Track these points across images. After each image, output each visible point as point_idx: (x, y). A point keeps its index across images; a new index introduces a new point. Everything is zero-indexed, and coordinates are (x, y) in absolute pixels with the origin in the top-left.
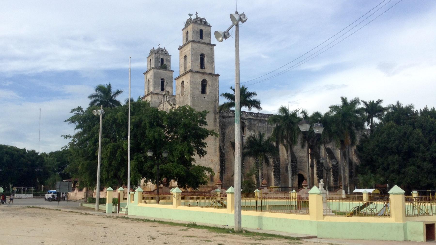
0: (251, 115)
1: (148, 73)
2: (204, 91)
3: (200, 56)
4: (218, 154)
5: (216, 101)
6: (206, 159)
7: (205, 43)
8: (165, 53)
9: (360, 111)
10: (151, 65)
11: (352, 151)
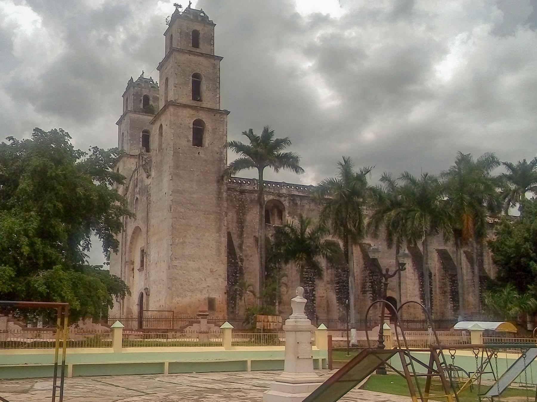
1: (123, 121)
2: (198, 141)
3: (191, 78)
4: (224, 257)
5: (222, 159)
6: (199, 268)
7: (202, 55)
9: (499, 181)
10: (127, 107)
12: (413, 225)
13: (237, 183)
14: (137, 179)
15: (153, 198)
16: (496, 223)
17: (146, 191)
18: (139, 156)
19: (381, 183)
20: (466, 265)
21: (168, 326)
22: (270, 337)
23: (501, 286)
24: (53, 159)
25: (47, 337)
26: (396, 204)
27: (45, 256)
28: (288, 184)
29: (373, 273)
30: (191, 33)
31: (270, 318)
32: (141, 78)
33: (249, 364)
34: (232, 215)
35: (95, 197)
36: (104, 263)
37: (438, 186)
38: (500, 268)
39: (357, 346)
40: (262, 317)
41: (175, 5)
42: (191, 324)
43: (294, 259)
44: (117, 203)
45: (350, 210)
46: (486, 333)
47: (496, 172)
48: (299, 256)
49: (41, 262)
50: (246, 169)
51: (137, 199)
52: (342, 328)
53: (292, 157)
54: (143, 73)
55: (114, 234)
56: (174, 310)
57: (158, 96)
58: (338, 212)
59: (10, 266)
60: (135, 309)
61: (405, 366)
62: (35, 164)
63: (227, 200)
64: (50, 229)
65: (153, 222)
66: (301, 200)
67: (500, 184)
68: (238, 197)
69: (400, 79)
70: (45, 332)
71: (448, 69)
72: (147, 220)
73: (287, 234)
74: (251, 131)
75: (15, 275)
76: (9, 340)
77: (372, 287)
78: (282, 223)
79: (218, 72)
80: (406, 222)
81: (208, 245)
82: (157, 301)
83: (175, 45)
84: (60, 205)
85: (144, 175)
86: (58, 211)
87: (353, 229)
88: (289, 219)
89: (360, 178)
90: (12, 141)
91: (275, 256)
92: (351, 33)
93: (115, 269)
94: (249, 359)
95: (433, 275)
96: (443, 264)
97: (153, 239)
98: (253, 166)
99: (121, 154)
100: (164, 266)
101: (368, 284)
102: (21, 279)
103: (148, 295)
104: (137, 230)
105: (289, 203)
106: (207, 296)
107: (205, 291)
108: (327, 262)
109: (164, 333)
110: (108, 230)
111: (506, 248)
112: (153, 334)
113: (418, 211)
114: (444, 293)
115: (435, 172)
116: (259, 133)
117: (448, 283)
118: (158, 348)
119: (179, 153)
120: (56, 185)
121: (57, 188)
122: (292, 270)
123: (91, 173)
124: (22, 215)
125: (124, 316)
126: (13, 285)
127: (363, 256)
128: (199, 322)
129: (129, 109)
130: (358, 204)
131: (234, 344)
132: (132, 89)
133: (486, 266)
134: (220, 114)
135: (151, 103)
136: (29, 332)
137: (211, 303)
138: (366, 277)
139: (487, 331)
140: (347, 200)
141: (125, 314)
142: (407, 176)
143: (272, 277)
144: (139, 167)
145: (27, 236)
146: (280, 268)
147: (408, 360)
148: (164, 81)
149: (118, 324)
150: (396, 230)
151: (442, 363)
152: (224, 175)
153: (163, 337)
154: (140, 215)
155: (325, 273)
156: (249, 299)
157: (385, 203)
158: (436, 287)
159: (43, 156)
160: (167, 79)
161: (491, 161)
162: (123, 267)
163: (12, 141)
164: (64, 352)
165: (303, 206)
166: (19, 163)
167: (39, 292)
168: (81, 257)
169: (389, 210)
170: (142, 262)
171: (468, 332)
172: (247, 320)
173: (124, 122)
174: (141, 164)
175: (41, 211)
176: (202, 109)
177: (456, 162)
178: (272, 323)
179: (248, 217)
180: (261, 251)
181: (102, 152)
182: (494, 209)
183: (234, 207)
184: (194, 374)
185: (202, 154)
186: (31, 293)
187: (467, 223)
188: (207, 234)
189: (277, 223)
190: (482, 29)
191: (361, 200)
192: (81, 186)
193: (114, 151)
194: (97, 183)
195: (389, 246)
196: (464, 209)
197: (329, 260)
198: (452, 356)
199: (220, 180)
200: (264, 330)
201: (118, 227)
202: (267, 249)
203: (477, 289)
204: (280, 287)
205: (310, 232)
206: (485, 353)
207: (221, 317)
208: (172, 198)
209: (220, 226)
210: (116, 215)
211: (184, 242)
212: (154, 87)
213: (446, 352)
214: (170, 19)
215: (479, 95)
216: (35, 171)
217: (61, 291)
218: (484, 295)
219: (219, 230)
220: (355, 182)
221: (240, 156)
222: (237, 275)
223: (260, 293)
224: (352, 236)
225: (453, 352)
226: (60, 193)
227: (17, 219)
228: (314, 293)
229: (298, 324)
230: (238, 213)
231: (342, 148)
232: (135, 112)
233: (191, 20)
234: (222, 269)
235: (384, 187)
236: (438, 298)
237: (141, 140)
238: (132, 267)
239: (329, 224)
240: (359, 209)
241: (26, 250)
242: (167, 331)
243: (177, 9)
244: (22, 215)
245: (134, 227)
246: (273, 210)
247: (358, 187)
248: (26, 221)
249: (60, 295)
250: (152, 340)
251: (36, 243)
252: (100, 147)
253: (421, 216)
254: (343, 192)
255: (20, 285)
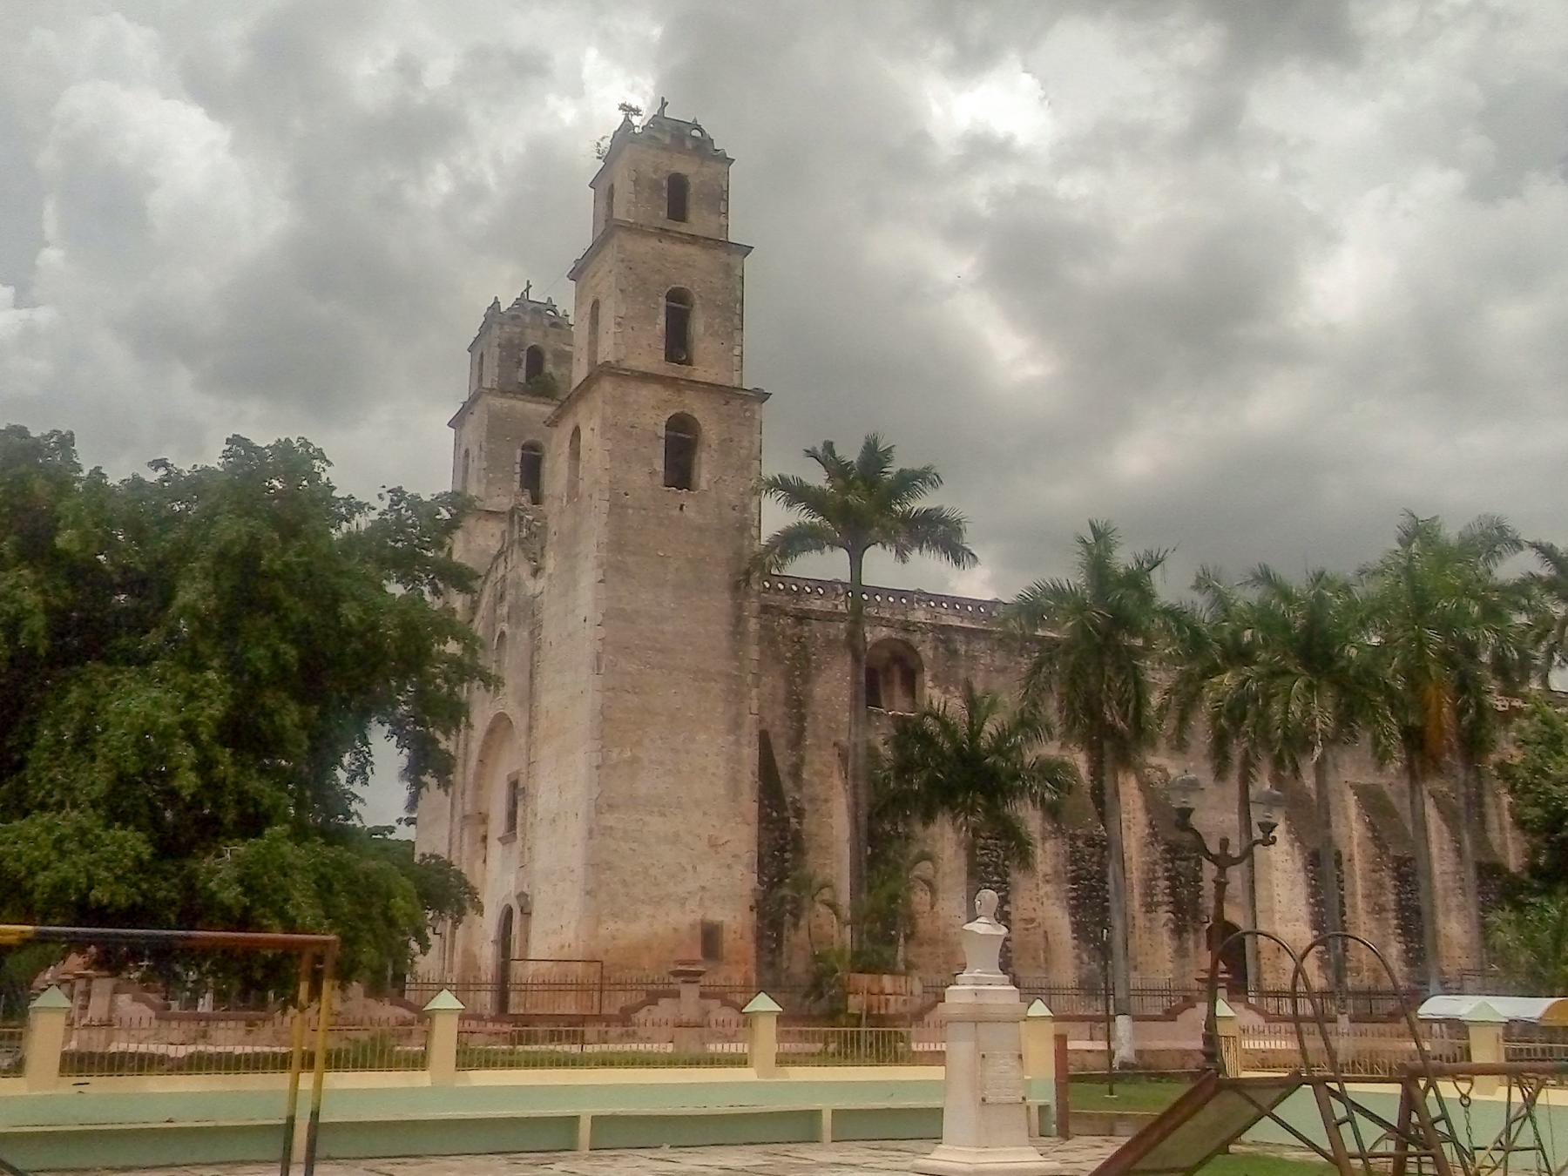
0: (958, 614)
2: (679, 472)
3: (663, 301)
4: (749, 804)
5: (746, 525)
6: (677, 835)
7: (693, 239)
8: (554, 325)
10: (480, 379)
11: (1498, 806)
12: (1286, 712)
13: (788, 591)
14: (504, 578)
15: (550, 633)
16: (1519, 712)
17: (528, 612)
18: (512, 515)
19: (1195, 596)
20: (1439, 831)
21: (593, 1009)
22: (879, 1038)
23: (1538, 893)
24: (276, 521)
25: (229, 1039)
26: (1239, 655)
27: (242, 798)
28: (932, 597)
29: (1173, 851)
30: (665, 183)
31: (887, 981)
32: (523, 301)
33: (827, 1119)
34: (773, 682)
35: (390, 630)
36: (399, 821)
37: (1352, 606)
38: (1535, 841)
39: (1134, 1066)
40: (865, 980)
41: (623, 107)
42: (653, 998)
43: (952, 809)
44: (452, 647)
45: (1109, 671)
46: (1513, 1029)
47: (1510, 568)
48: (965, 801)
49: (230, 816)
50: (815, 554)
51: (502, 634)
52: (1090, 1013)
53: (945, 521)
54: (529, 287)
55: (439, 735)
56: (604, 958)
57: (568, 348)
58: (1074, 678)
59: (139, 828)
60: (487, 955)
61: (1332, 1126)
62: (226, 537)
63: (761, 638)
64: (261, 720)
65: (548, 700)
66: (968, 644)
67: (1524, 602)
68: (789, 632)
69: (1210, 314)
70: (222, 1025)
71: (1345, 284)
72: (530, 697)
73: (926, 739)
74: (829, 446)
75: (153, 855)
76: (113, 1048)
77: (1173, 893)
78: (914, 706)
79: (739, 286)
80: (1267, 704)
81: (704, 769)
82: (554, 932)
83: (620, 213)
84: (291, 653)
85: (525, 570)
86: (284, 669)
87: (1121, 725)
88: (932, 694)
89: (1136, 581)
90: (162, 472)
91: (894, 800)
92: (1076, 188)
93: (432, 838)
94: (826, 1106)
95: (1345, 858)
96: (1371, 826)
97: (546, 752)
98: (834, 544)
99: (461, 505)
100: (576, 829)
101: (1163, 884)
102: (169, 866)
103: (526, 914)
104: (501, 723)
105: (936, 648)
106: (698, 917)
107: (692, 904)
108: (1044, 819)
109: (571, 1028)
110: (423, 723)
111: (1548, 784)
112: (541, 1029)
113: (1299, 676)
114: (1378, 910)
115: (1342, 568)
116: (850, 453)
117: (1389, 883)
118: (554, 1071)
119: (625, 507)
120: (282, 593)
121: (286, 604)
122: (945, 842)
123: (382, 563)
124: (180, 679)
125: (454, 977)
126: (145, 886)
127: (1146, 801)
128: (677, 995)
129: (487, 384)
130: (1133, 653)
131: (783, 1060)
132: (496, 331)
133: (1494, 836)
134: (743, 400)
135: (549, 367)
136: (174, 1024)
137: (710, 937)
138: (1155, 863)
139: (1510, 1025)
140: (1100, 644)
141: (456, 971)
142: (1264, 577)
143: (887, 862)
144: (511, 545)
145: (192, 738)
146: (907, 837)
147: (1340, 1110)
148: (587, 309)
149: (446, 1001)
150: (1238, 728)
151: (1437, 1120)
152: (752, 572)
153: (576, 1038)
154: (513, 680)
155: (1039, 852)
156: (830, 925)
157: (1204, 651)
158: (1353, 894)
159: (248, 514)
160: (596, 305)
161: (1495, 538)
162: (457, 832)
163: (162, 472)
164: (318, 1083)
165: (975, 658)
166: (178, 533)
167: (222, 903)
168: (339, 802)
169: (1217, 670)
170: (512, 817)
171: (1457, 1026)
172: (817, 987)
173: (478, 417)
174: (516, 536)
175: (235, 668)
176: (693, 384)
177: (1400, 541)
178: (892, 998)
179: (820, 690)
180: (855, 787)
181: (415, 503)
182: (1510, 672)
183: (778, 659)
184: (665, 1152)
185: (691, 508)
186: (196, 909)
187: (1440, 711)
188: (702, 737)
189: (899, 706)
190: (1436, 184)
191: (1139, 642)
192: (354, 598)
193: (441, 500)
194: (396, 589)
195: (1220, 773)
196: (1426, 669)
197: (1052, 812)
198: (1464, 1096)
199: (739, 585)
200: (869, 1016)
201: (454, 714)
202: (874, 784)
203: (1471, 900)
204: (909, 889)
205: (994, 732)
206: (1516, 1091)
207: (737, 979)
208: (602, 632)
209: (739, 714)
210: (447, 680)
211: (635, 760)
212: (558, 324)
213: (1447, 1089)
214: (607, 143)
215: (1436, 359)
216: (222, 556)
217: (286, 900)
218: (1492, 918)
219: (735, 725)
220: (1122, 591)
221: (797, 516)
222: (788, 855)
223: (853, 909)
224: (1115, 739)
225: (1464, 1087)
226: (294, 618)
227: (167, 691)
228: (1006, 908)
229: (988, 1000)
230: (788, 677)
231: (1065, 497)
232: (503, 391)
233: (665, 148)
234: (742, 837)
235: (1202, 608)
236: (1362, 923)
237: (518, 470)
238: (481, 830)
239: (1051, 708)
240: (1135, 667)
241: (188, 781)
242: (583, 1020)
243: (627, 120)
244: (180, 679)
245: (491, 714)
246: (887, 670)
247: (1131, 602)
248: (192, 696)
249: (281, 914)
250: (535, 1048)
251: (218, 762)
252: (410, 490)
253: (1309, 687)
254: (1089, 620)
255: (164, 885)
